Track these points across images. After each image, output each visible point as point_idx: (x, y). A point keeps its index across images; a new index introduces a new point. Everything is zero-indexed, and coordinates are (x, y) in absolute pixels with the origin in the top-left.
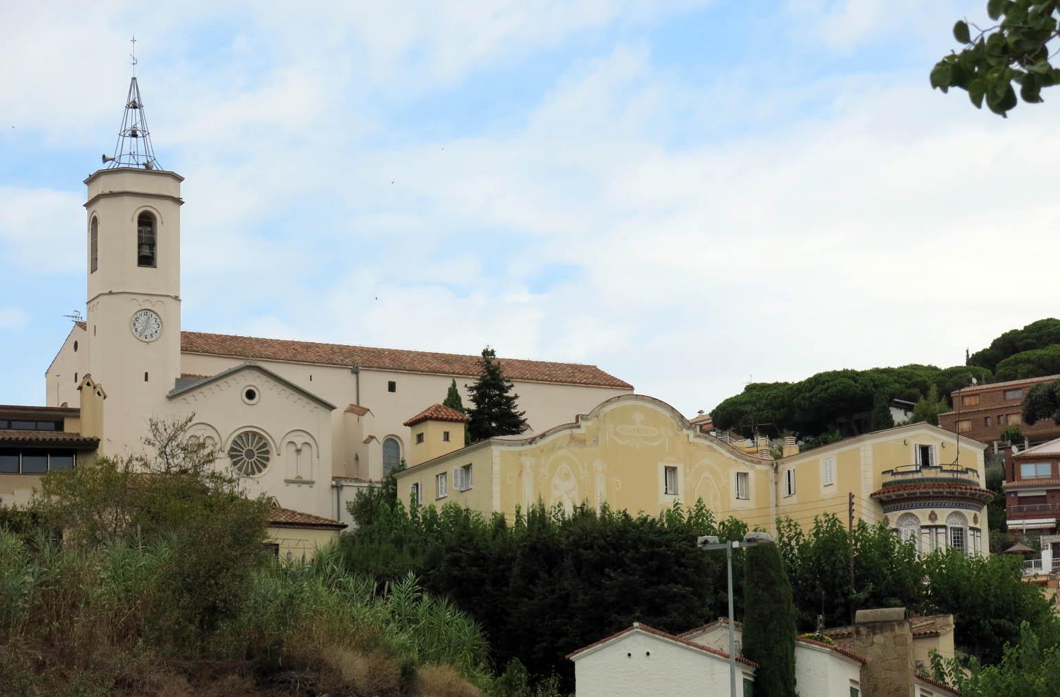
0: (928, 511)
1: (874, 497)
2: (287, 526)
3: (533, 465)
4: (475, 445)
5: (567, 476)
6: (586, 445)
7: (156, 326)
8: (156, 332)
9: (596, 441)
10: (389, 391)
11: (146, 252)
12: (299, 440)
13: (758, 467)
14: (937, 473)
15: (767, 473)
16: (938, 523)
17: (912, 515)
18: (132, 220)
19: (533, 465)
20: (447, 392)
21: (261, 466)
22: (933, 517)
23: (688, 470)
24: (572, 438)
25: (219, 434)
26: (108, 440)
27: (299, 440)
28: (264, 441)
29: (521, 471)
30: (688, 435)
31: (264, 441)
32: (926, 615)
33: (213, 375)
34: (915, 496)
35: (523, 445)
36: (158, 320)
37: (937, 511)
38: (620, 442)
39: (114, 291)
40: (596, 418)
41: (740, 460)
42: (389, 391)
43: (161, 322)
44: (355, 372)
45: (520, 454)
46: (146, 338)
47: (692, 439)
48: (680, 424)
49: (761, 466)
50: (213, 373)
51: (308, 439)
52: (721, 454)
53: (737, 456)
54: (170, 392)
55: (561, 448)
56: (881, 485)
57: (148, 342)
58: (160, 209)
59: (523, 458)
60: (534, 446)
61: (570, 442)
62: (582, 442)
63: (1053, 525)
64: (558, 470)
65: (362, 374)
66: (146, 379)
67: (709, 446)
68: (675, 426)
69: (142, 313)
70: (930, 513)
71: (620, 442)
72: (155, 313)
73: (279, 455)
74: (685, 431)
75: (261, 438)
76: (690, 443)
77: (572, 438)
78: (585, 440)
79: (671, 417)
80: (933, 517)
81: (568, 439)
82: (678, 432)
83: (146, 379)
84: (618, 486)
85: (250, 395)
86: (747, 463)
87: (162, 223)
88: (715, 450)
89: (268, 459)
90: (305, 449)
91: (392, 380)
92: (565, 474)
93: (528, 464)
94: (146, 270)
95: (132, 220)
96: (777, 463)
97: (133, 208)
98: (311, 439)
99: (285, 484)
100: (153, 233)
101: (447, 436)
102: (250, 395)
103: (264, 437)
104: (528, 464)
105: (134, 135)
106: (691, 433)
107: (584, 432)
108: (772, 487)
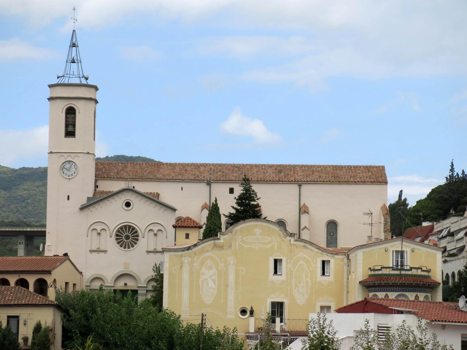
0: (414, 294)
1: (361, 283)
2: (24, 306)
3: (190, 262)
4: (206, 240)
5: (210, 268)
6: (223, 249)
7: (74, 170)
8: (75, 173)
9: (230, 247)
10: (230, 193)
11: (70, 129)
12: (155, 228)
13: (336, 257)
14: (390, 271)
15: (342, 260)
18: (62, 112)
19: (190, 262)
21: (124, 245)
23: (289, 261)
25: (109, 228)
26: (48, 233)
27: (155, 228)
28: (135, 230)
29: (182, 266)
30: (290, 240)
31: (135, 230)
33: (114, 191)
35: (183, 251)
36: (76, 167)
37: (419, 294)
38: (245, 246)
39: (53, 152)
40: (230, 233)
41: (324, 253)
42: (230, 193)
43: (77, 167)
44: (209, 184)
45: (182, 256)
46: (69, 176)
47: (292, 242)
48: (285, 234)
49: (339, 256)
51: (160, 228)
52: (312, 250)
53: (322, 251)
54: (81, 206)
55: (207, 251)
56: (368, 276)
57: (69, 179)
58: (80, 107)
59: (183, 259)
60: (190, 251)
61: (213, 248)
62: (221, 247)
64: (205, 263)
66: (68, 199)
67: (304, 246)
68: (282, 235)
69: (67, 163)
70: (385, 295)
71: (245, 246)
72: (74, 163)
73: (143, 237)
74: (288, 238)
75: (134, 228)
76: (291, 244)
78: (223, 246)
79: (279, 230)
81: (212, 246)
82: (284, 239)
83: (68, 199)
84: (243, 272)
85: (128, 204)
86: (329, 255)
87: (79, 112)
88: (308, 248)
89: (137, 240)
90: (159, 233)
91: (232, 187)
92: (209, 266)
93: (186, 261)
94: (70, 140)
95: (62, 112)
96: (348, 254)
97: (63, 106)
98: (163, 227)
99: (146, 253)
101: (187, 236)
102: (128, 204)
103: (136, 228)
104: (186, 261)
106: (292, 239)
107: (223, 242)
108: (345, 268)
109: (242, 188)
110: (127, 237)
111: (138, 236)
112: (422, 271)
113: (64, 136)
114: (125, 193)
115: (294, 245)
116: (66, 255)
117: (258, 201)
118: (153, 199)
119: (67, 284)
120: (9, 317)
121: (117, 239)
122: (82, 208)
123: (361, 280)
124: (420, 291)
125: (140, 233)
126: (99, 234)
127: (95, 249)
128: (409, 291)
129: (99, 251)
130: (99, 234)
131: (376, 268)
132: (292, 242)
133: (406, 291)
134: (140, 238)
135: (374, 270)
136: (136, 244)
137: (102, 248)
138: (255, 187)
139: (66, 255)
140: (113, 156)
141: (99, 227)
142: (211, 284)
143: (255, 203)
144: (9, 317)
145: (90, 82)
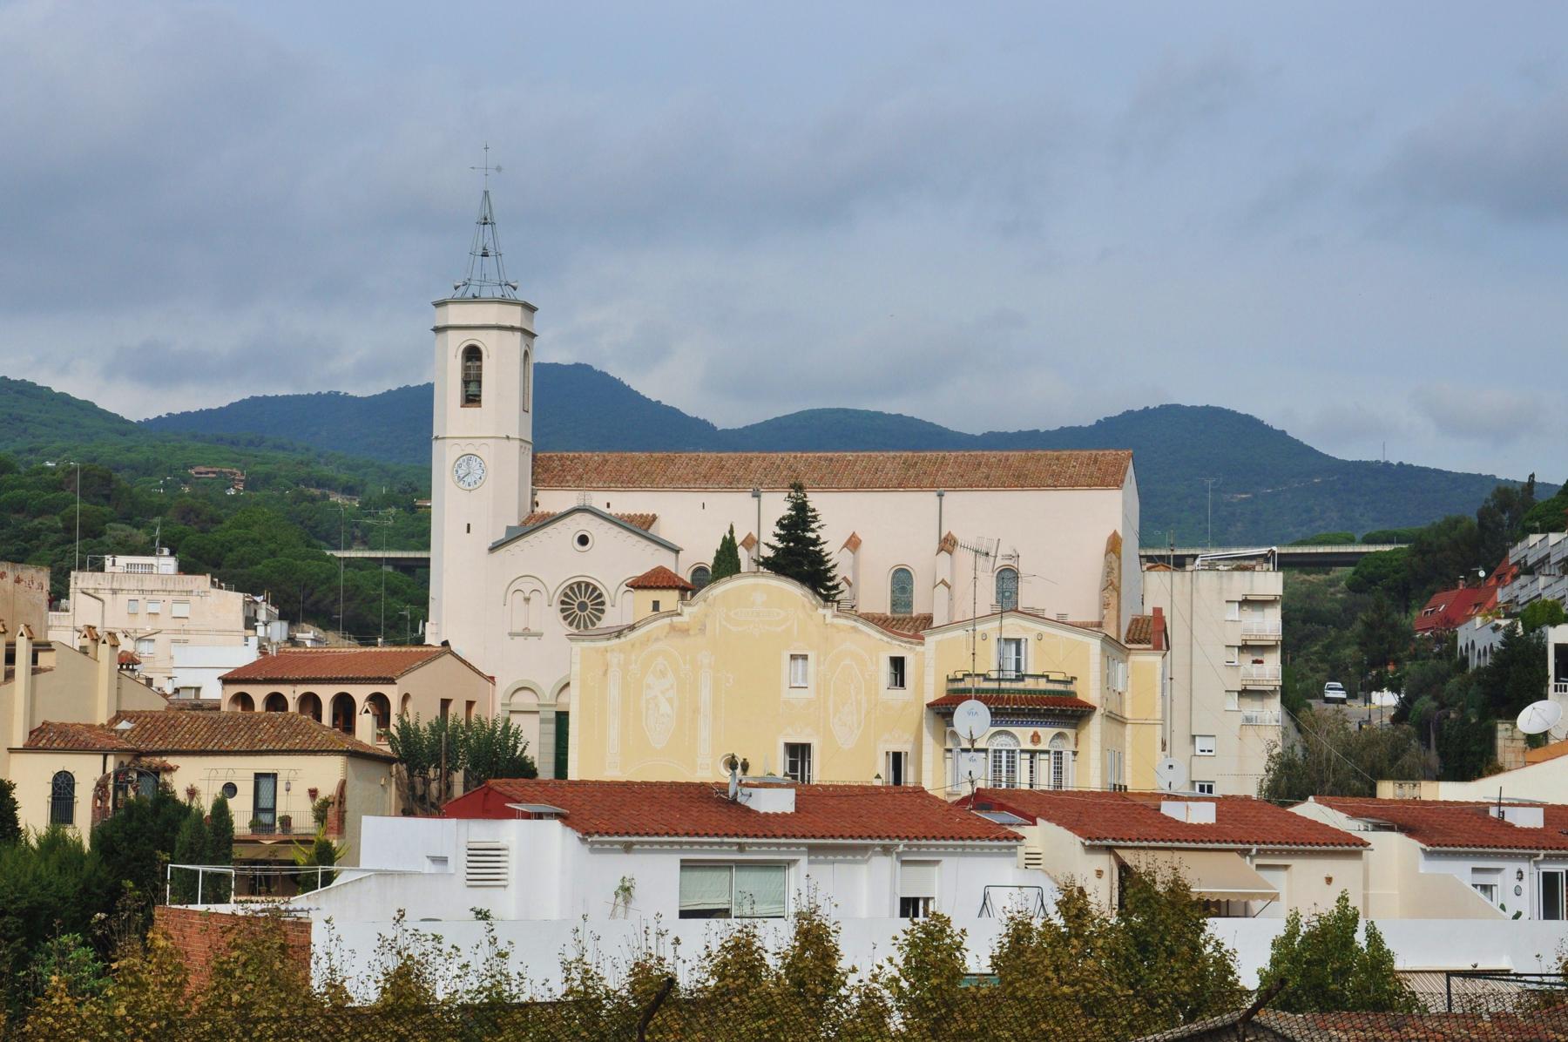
0: (1030, 730)
5: (663, 674)
9: (702, 630)
11: (473, 388)
16: (1039, 747)
17: (1008, 733)
20: (720, 542)
22: (1036, 738)
24: (672, 627)
32: (1331, 794)
34: (287, 871)
37: (1041, 730)
44: (756, 495)
47: (829, 619)
50: (560, 510)
55: (657, 639)
62: (684, 631)
63: (1017, 786)
65: (764, 496)
67: (853, 628)
77: (672, 627)
80: (1036, 738)
85: (583, 540)
89: (602, 611)
94: (472, 411)
97: (456, 343)
100: (466, 369)
102: (583, 540)
105: (485, 255)
109: (789, 505)
110: (583, 607)
111: (603, 603)
112: (1049, 681)
113: (459, 403)
114: (577, 516)
115: (832, 625)
116: (445, 644)
117: (820, 532)
118: (641, 526)
119: (445, 703)
120: (258, 776)
121: (563, 610)
122: (494, 548)
123: (931, 700)
124: (1043, 724)
125: (606, 598)
126: (527, 600)
127: (520, 630)
128: (1018, 724)
129: (526, 633)
130: (527, 600)
131: (960, 676)
132: (829, 619)
133: (1012, 724)
134: (607, 608)
135: (956, 680)
136: (565, 618)
137: (533, 629)
138: (815, 500)
139: (445, 644)
140: (1042, 430)
141: (527, 587)
142: (665, 707)
143: (812, 535)
144: (258, 776)
145: (521, 296)
